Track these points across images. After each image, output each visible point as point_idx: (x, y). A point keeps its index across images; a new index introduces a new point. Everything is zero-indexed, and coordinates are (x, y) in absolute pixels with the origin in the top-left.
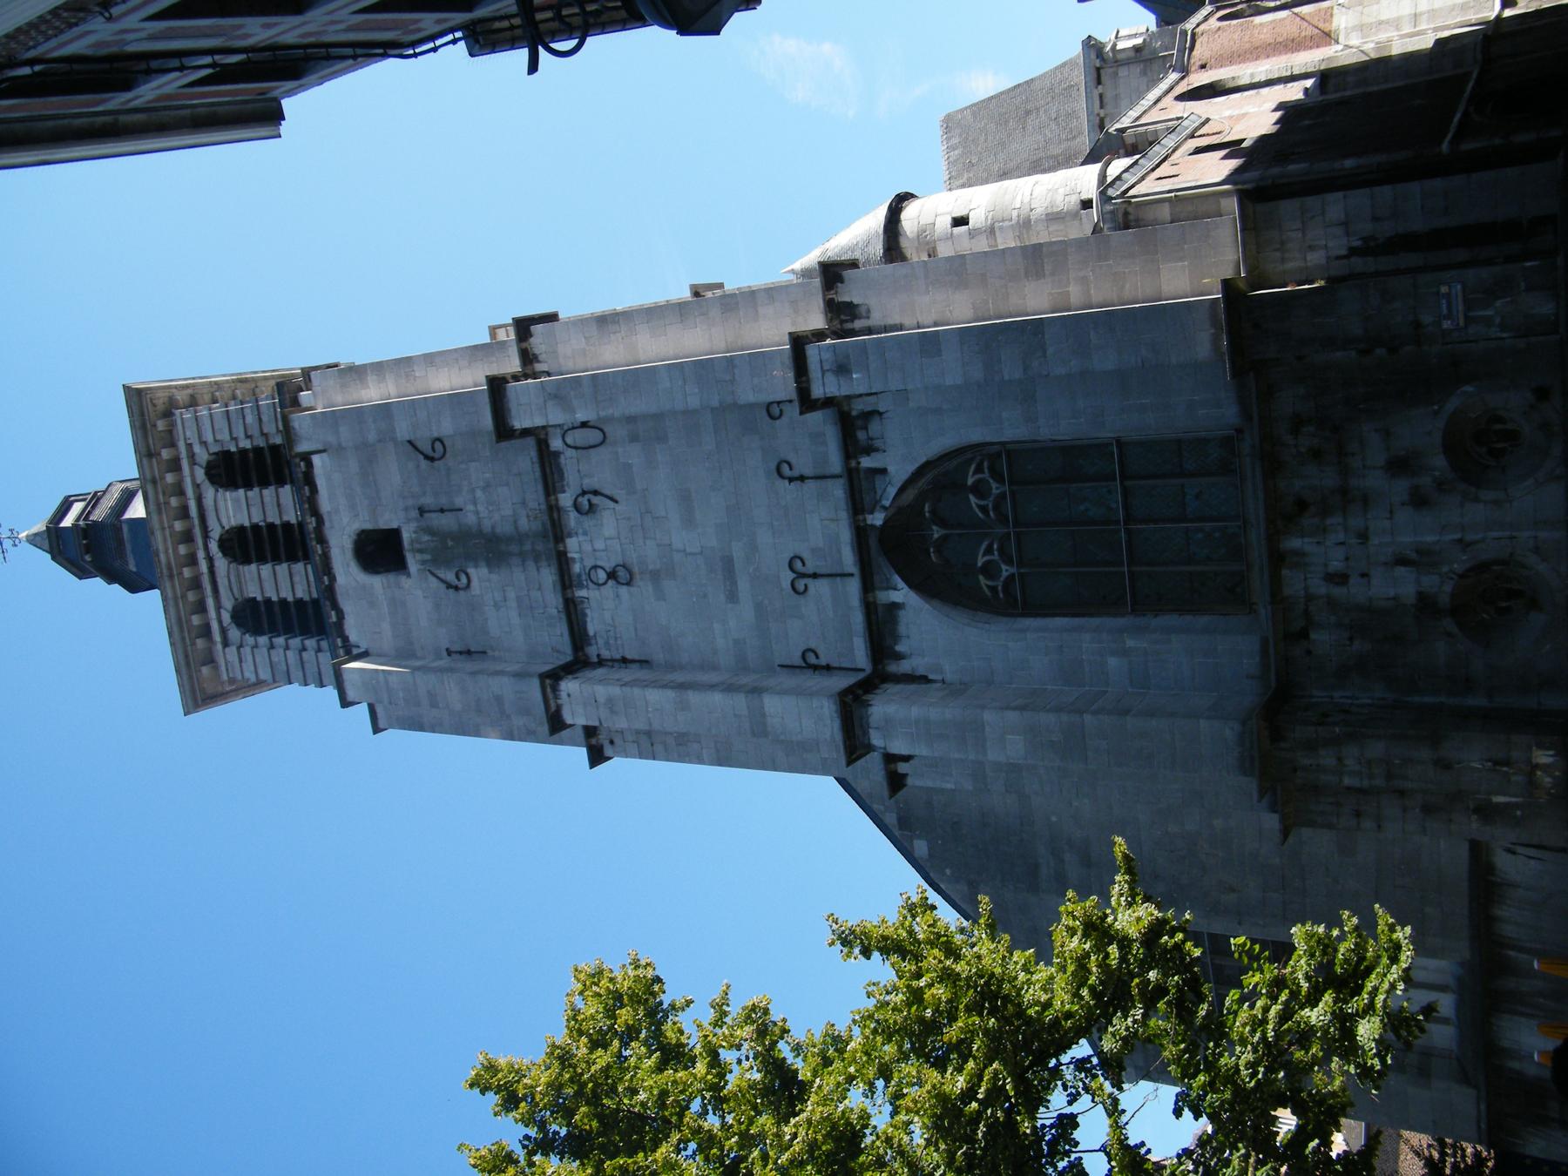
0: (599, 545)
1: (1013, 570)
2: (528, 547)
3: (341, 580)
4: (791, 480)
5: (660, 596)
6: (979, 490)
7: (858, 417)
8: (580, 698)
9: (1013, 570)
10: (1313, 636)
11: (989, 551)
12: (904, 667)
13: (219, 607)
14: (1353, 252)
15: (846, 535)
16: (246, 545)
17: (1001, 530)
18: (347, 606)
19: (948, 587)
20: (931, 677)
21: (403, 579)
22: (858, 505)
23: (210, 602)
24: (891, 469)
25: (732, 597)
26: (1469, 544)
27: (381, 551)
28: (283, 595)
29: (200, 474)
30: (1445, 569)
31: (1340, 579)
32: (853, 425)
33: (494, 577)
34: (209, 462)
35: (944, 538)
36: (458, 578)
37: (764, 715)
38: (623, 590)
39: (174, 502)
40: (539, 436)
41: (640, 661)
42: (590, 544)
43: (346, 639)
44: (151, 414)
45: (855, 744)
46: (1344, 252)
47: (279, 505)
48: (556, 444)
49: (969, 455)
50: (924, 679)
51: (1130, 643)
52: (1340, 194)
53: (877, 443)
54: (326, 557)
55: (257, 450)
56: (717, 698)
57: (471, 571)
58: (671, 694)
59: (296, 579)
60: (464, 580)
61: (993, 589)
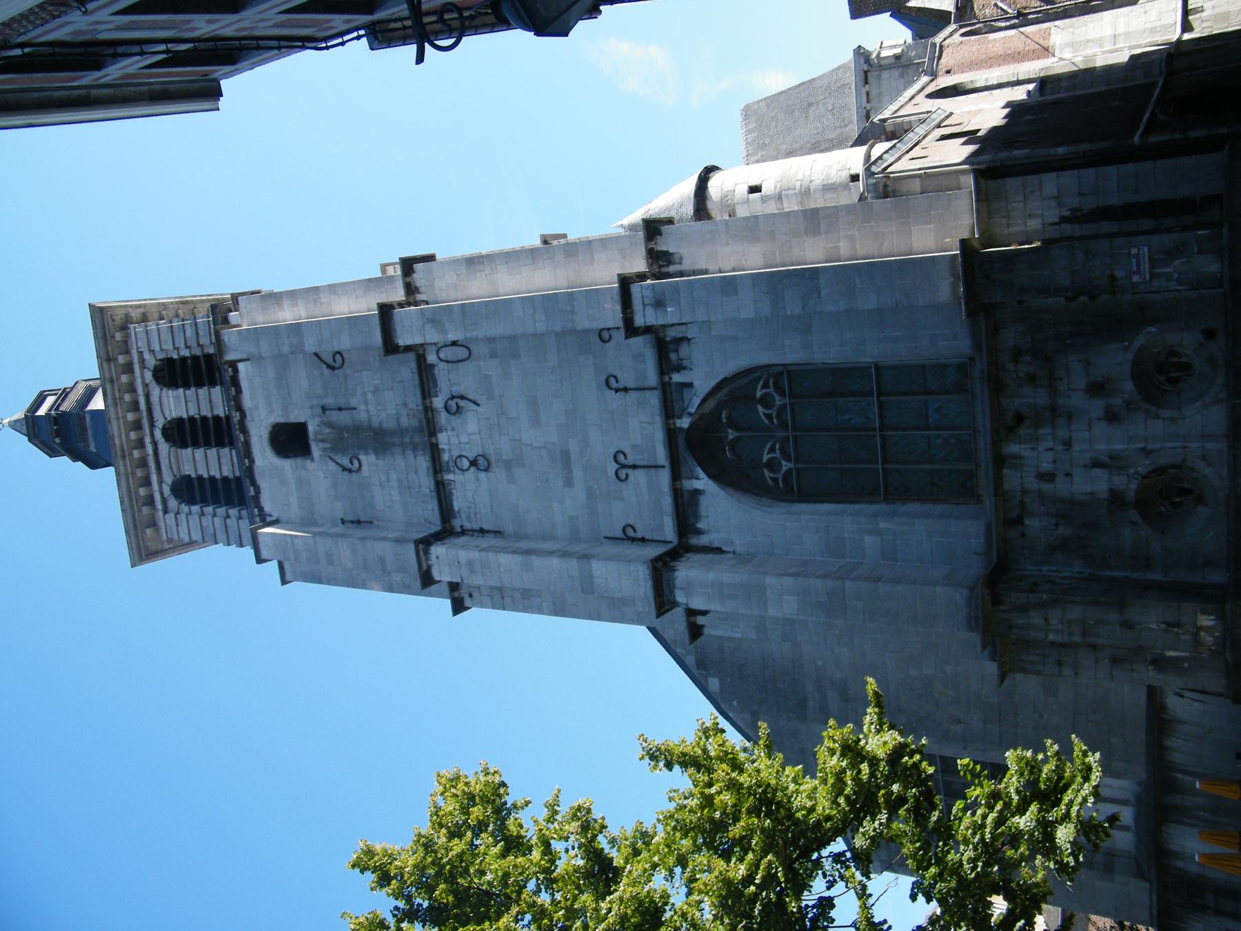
1: (791, 465)
2: (407, 439)
3: (259, 462)
4: (617, 390)
5: (511, 480)
6: (766, 402)
7: (671, 342)
9: (791, 465)
10: (1027, 522)
11: (772, 450)
12: (703, 540)
13: (161, 482)
14: (1063, 220)
15: (659, 435)
16: (184, 433)
17: (784, 434)
19: (739, 478)
20: (725, 549)
22: (669, 411)
23: (154, 478)
25: (569, 482)
26: (1151, 452)
27: (290, 440)
28: (212, 473)
29: (149, 376)
30: (1131, 471)
31: (1049, 477)
33: (380, 463)
34: (156, 367)
35: (737, 439)
36: (352, 463)
37: (591, 576)
38: (483, 475)
39: (127, 397)
40: (419, 352)
42: (458, 438)
43: (261, 509)
44: (111, 328)
45: (663, 601)
46: (1056, 220)
48: (431, 358)
49: (758, 374)
50: (719, 550)
51: (882, 525)
52: (1054, 175)
53: (685, 363)
54: (247, 444)
56: (555, 562)
57: (362, 457)
58: (518, 558)
59: (223, 460)
60: (356, 464)
61: (775, 480)
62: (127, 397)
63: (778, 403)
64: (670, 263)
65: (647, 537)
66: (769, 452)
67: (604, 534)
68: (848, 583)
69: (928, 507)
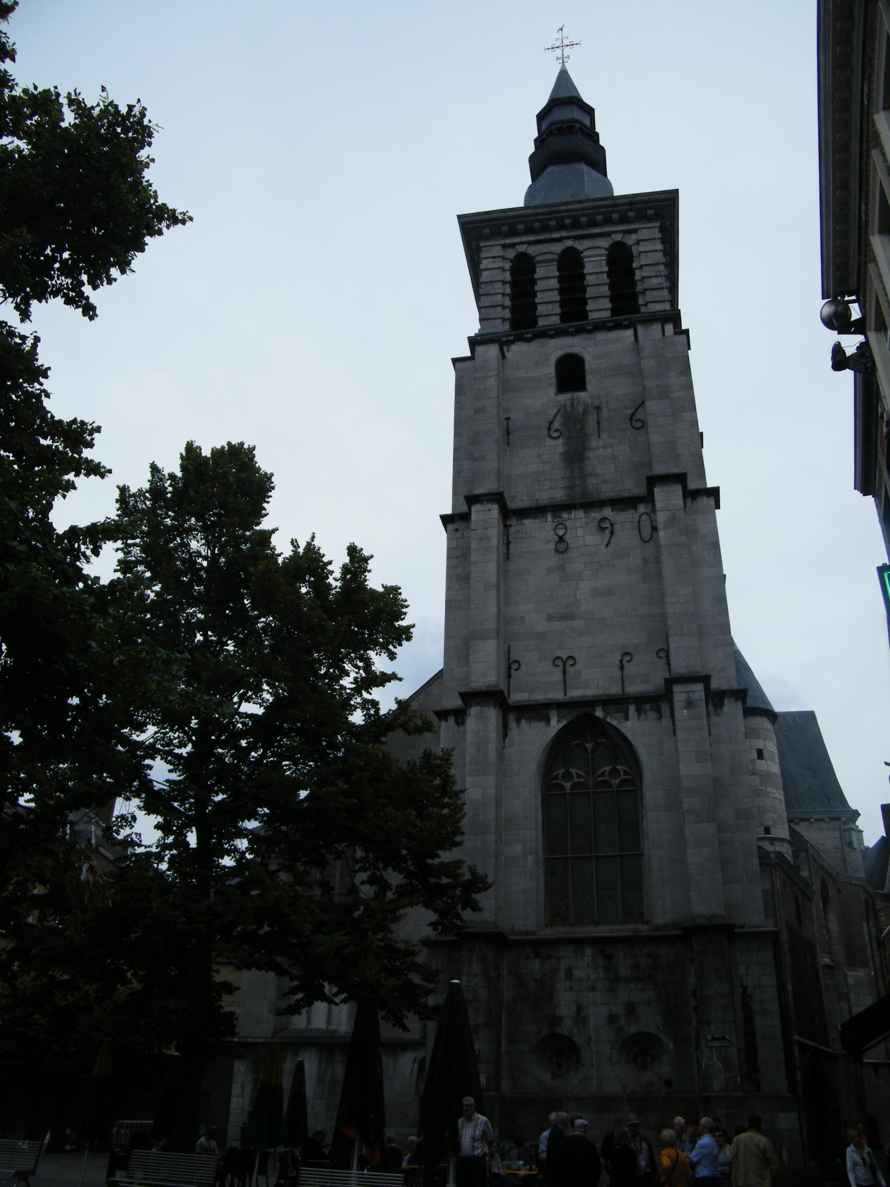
0: (580, 532)
1: (568, 790)
2: (577, 482)
3: (552, 343)
4: (621, 661)
6: (614, 771)
8: (486, 516)
9: (568, 790)
10: (537, 961)
11: (579, 776)
12: (512, 724)
13: (529, 243)
14: (745, 989)
15: (589, 692)
16: (571, 266)
18: (534, 346)
19: (558, 750)
21: (553, 390)
24: (628, 723)
25: (550, 618)
27: (571, 374)
28: (539, 295)
29: (618, 237)
30: (575, 1031)
31: (569, 975)
32: (656, 701)
33: (558, 456)
35: (586, 750)
36: (556, 430)
38: (552, 546)
39: (600, 218)
40: (649, 498)
41: (508, 554)
42: (580, 528)
44: (661, 208)
45: (471, 697)
46: (745, 984)
47: (598, 297)
48: (642, 508)
50: (505, 736)
51: (530, 858)
52: (775, 983)
53: (643, 715)
55: (634, 284)
56: (494, 610)
57: (560, 441)
58: (494, 579)
59: (550, 306)
60: (555, 435)
61: (556, 777)
62: (600, 218)
63: (613, 781)
64: (715, 706)
65: (512, 680)
66: (577, 774)
67: (512, 644)
68: (493, 836)
69: (542, 890)
